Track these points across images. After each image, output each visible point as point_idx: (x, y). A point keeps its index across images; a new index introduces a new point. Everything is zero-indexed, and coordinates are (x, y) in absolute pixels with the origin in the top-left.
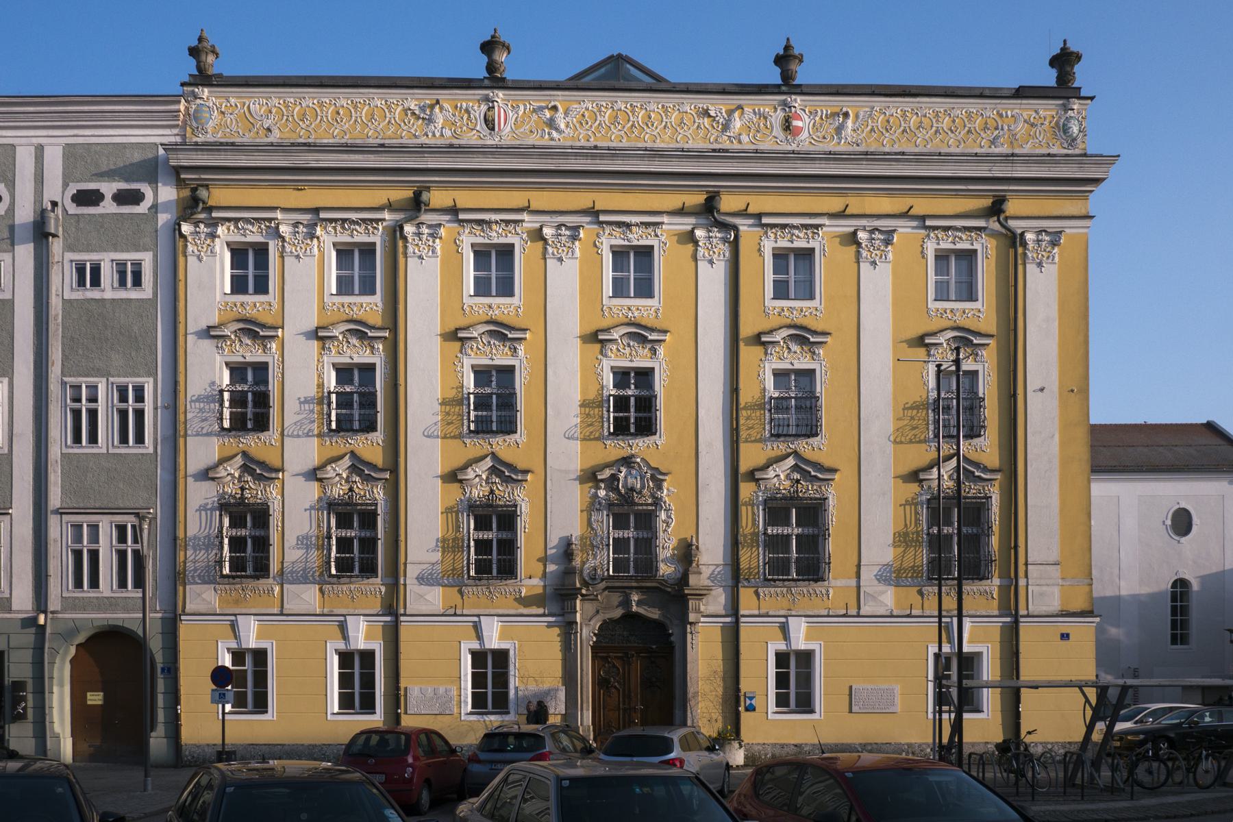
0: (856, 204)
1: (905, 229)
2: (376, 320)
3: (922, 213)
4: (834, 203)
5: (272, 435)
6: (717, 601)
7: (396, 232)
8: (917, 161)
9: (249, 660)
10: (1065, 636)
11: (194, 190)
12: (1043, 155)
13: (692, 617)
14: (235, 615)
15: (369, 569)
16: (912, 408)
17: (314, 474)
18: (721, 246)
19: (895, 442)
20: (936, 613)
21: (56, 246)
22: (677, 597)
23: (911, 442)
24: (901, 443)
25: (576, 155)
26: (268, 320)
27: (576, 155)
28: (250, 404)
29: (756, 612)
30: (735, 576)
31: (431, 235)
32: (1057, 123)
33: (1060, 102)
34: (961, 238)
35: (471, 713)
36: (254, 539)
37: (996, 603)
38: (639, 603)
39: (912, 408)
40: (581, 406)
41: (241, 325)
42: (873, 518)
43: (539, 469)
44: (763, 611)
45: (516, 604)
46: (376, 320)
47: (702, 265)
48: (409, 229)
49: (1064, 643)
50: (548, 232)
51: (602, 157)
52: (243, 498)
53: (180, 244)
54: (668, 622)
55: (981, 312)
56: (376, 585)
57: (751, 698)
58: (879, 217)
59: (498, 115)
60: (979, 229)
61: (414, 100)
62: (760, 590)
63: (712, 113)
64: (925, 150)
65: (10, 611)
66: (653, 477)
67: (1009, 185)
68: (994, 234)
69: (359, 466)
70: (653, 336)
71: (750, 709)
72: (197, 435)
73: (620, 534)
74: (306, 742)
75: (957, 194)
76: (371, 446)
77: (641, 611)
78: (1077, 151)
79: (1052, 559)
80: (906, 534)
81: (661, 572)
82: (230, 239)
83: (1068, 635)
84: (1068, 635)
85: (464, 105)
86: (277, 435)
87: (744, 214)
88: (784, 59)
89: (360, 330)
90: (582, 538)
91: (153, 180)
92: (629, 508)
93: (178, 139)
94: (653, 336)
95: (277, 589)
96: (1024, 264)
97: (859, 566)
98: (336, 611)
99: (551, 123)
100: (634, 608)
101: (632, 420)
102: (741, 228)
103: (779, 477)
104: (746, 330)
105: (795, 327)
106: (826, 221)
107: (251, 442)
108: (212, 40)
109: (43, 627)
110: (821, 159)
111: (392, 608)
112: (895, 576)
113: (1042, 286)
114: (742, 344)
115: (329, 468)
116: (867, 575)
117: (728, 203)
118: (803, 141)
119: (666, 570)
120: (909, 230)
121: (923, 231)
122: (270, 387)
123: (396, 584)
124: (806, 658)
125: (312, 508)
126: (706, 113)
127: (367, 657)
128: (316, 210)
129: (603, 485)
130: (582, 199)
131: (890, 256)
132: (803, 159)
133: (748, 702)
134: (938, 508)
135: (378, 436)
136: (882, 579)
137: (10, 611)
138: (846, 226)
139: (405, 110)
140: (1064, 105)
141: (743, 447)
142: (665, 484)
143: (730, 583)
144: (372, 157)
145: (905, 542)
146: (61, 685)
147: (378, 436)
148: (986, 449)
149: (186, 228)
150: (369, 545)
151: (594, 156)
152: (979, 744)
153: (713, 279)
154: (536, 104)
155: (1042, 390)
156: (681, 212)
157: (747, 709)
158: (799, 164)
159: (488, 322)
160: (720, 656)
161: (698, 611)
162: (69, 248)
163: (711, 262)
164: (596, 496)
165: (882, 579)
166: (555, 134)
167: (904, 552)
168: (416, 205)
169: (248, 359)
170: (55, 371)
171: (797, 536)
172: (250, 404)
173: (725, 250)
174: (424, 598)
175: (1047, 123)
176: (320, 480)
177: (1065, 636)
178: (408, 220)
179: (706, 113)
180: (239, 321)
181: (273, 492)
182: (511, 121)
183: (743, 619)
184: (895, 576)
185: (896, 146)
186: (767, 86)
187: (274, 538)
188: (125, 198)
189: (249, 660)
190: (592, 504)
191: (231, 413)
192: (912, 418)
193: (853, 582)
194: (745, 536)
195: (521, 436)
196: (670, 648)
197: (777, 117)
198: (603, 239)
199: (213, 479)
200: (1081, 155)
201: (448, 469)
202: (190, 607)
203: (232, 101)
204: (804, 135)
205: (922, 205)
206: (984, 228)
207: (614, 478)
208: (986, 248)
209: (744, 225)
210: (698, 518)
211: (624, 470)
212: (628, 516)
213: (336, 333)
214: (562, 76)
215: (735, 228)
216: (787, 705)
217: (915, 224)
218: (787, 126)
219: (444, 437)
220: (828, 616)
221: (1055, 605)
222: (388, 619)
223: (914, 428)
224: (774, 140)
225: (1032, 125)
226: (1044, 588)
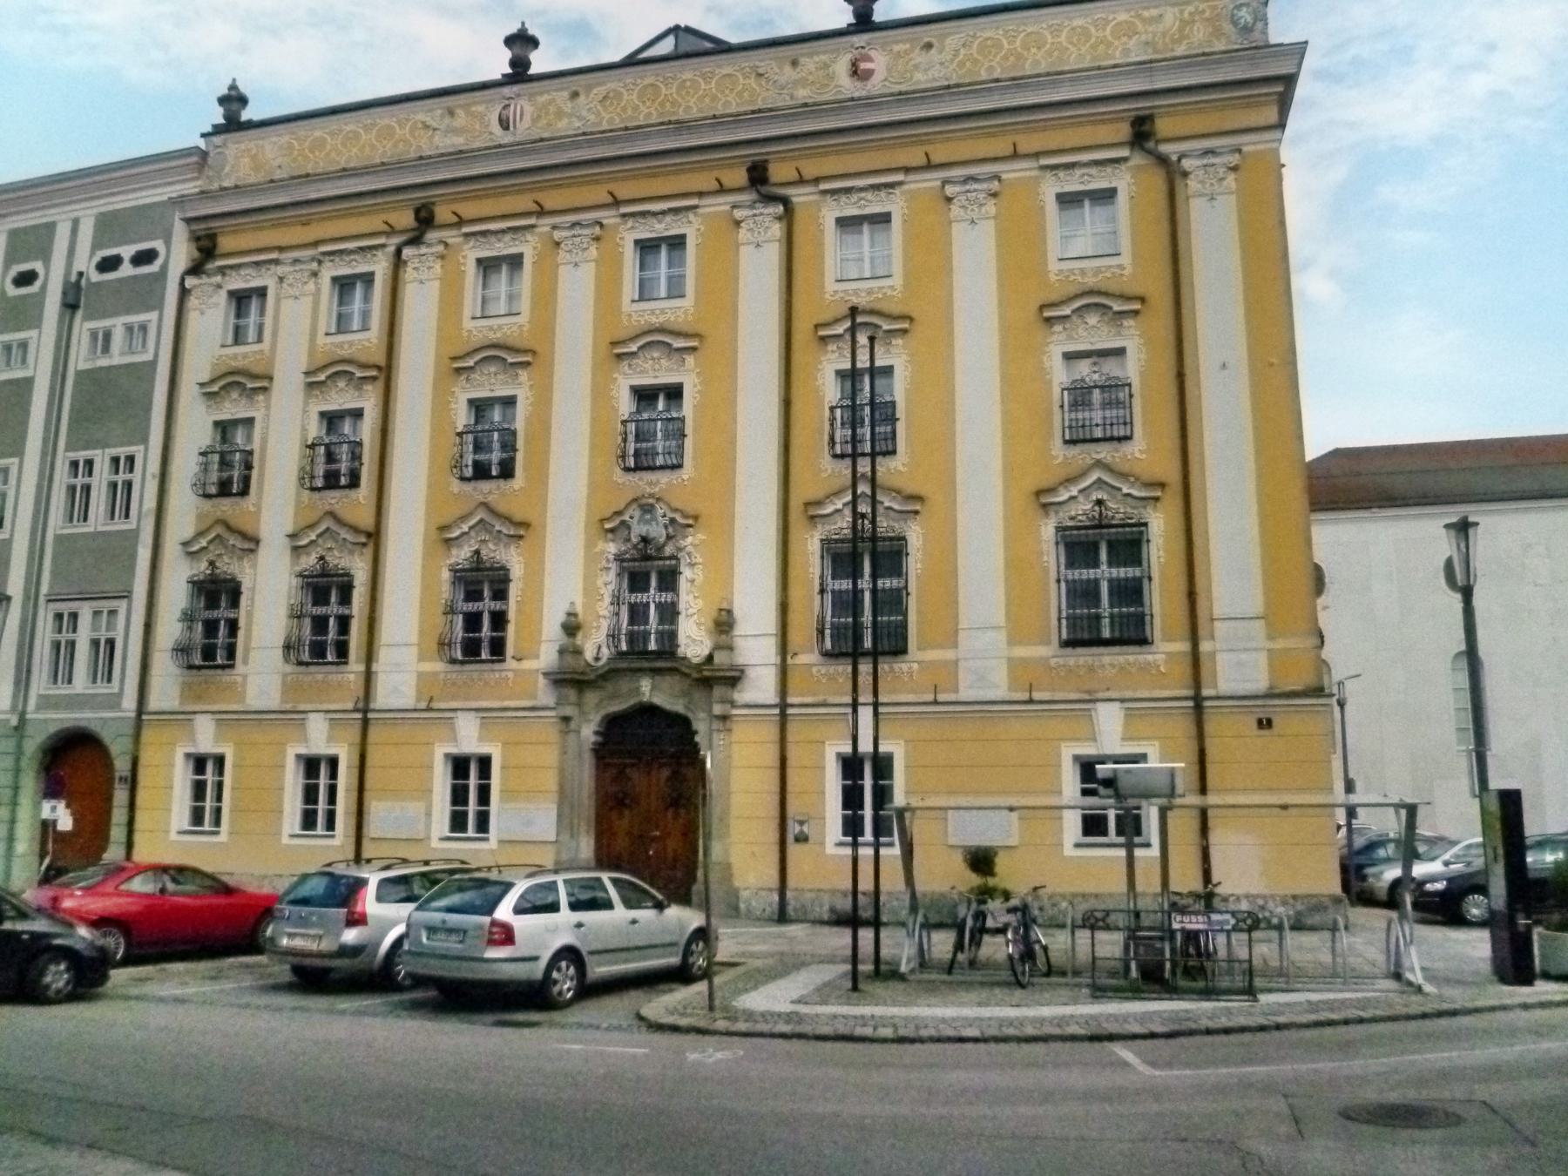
15: (1134, 634)
20: (848, 699)
35: (1078, 845)
36: (659, 606)
54: (690, 715)
57: (801, 823)
71: (802, 839)
73: (471, 607)
75: (1078, 122)
84: (1269, 723)
88: (521, 42)
98: (831, 700)
102: (795, 200)
105: (1091, 292)
107: (225, 506)
113: (1213, 224)
117: (779, 172)
118: (875, 85)
124: (485, 763)
133: (797, 828)
134: (1078, 547)
148: (1146, 450)
150: (1130, 592)
155: (1224, 366)
157: (797, 840)
162: (87, 318)
168: (425, 220)
204: (876, 79)
209: (799, 196)
212: (647, 576)
215: (785, 201)
224: (847, 86)
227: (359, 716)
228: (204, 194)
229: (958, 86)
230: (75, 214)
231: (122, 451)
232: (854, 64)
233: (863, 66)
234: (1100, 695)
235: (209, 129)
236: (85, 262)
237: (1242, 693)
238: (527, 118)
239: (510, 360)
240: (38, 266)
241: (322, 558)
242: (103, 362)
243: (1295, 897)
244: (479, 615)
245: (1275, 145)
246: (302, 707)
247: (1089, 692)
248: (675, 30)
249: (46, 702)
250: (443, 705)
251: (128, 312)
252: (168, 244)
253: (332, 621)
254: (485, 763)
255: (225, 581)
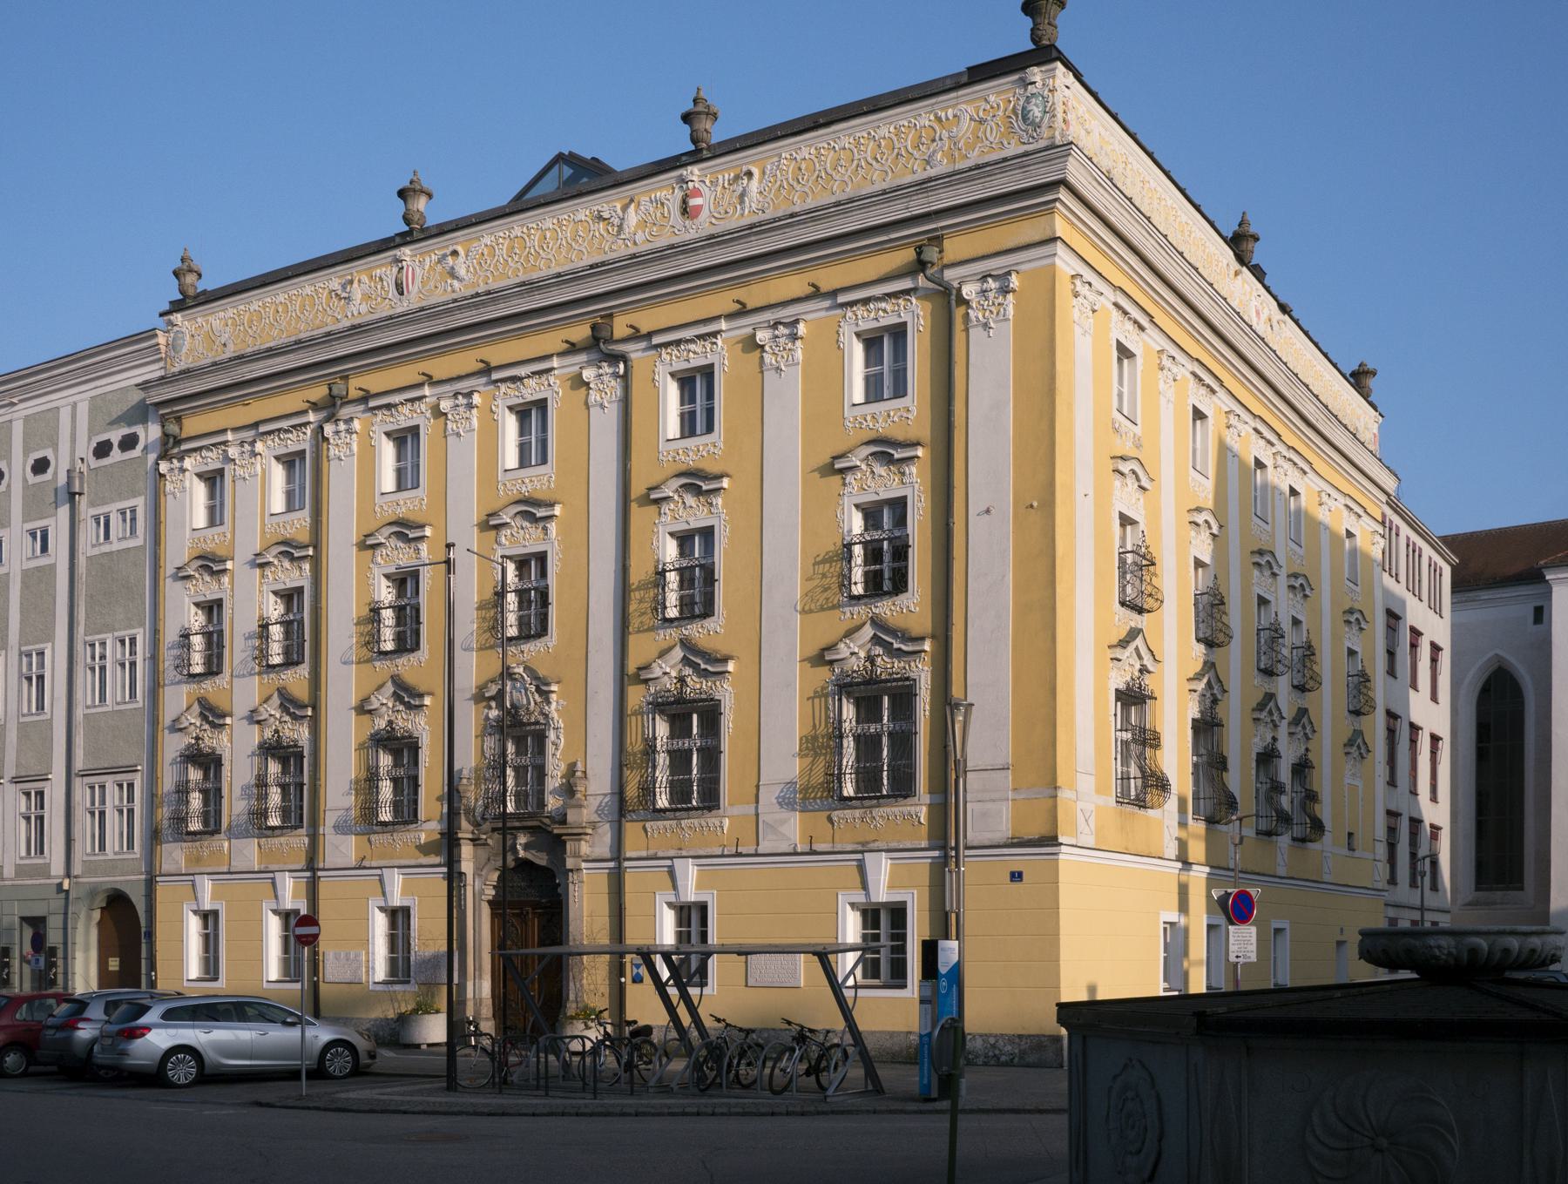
0: (754, 295)
1: (814, 312)
2: (304, 537)
3: (251, 421)
4: (724, 301)
5: (223, 680)
6: (598, 844)
7: (320, 437)
8: (813, 219)
9: (884, 919)
10: (1016, 876)
11: (919, 251)
12: (971, 169)
13: (570, 863)
14: (671, 858)
16: (824, 561)
17: (253, 718)
18: (613, 383)
19: (803, 612)
21: (83, 502)
22: (554, 838)
23: (822, 609)
24: (811, 611)
25: (459, 308)
26: (221, 552)
27: (459, 308)
28: (887, 558)
29: (644, 854)
30: (621, 809)
31: (347, 431)
32: (1014, 111)
33: (1015, 77)
34: (885, 311)
37: (924, 830)
38: (526, 847)
39: (824, 561)
40: (478, 609)
41: (200, 563)
42: (774, 720)
43: (441, 692)
44: (651, 852)
45: (417, 853)
46: (304, 537)
47: (594, 411)
48: (329, 429)
49: (1016, 885)
50: (762, 336)
51: (483, 304)
52: (199, 750)
53: (959, 312)
55: (910, 412)
56: (299, 840)
58: (460, 378)
59: (408, 277)
60: (907, 292)
61: (332, 280)
62: (648, 825)
63: (606, 215)
64: (885, 186)
65: (49, 877)
66: (538, 690)
67: (1042, 195)
68: (926, 296)
69: (289, 703)
70: (540, 513)
72: (639, 631)
74: (1009, 1030)
75: (881, 248)
76: (296, 680)
77: (529, 856)
78: (1042, 144)
79: (999, 762)
80: (815, 738)
81: (549, 808)
82: (198, 470)
83: (1020, 874)
84: (1020, 874)
85: (950, 112)
86: (227, 678)
87: (636, 336)
89: (886, 450)
90: (477, 769)
91: (144, 420)
92: (519, 731)
93: (162, 373)
94: (540, 513)
95: (226, 844)
96: (967, 330)
97: (758, 787)
98: (660, 854)
99: (452, 274)
100: (522, 854)
101: (886, 575)
102: (633, 356)
103: (667, 671)
104: (637, 489)
106: (723, 325)
108: (714, 101)
109: (67, 892)
110: (702, 247)
111: (945, 835)
112: (802, 798)
113: (989, 359)
114: (634, 506)
115: (842, 645)
116: (768, 797)
119: (552, 803)
120: (823, 314)
121: (839, 311)
122: (909, 531)
123: (945, 805)
124: (703, 908)
125: (253, 754)
126: (600, 218)
127: (898, 913)
128: (256, 425)
129: (493, 704)
130: (466, 361)
131: (799, 355)
132: (683, 252)
135: (304, 670)
136: (786, 803)
137: (49, 877)
138: (744, 326)
139: (331, 292)
140: (1021, 79)
141: (633, 640)
142: (554, 697)
143: (616, 817)
144: (291, 356)
145: (813, 749)
146: (87, 950)
147: (304, 670)
149: (164, 467)
151: (476, 306)
152: (899, 1033)
153: (605, 424)
154: (440, 253)
155: (988, 511)
156: (573, 349)
157: (634, 981)
158: (682, 260)
159: (868, 443)
160: (607, 912)
161: (577, 855)
162: (92, 504)
163: (602, 406)
164: (487, 718)
165: (786, 803)
166: (456, 283)
167: (813, 763)
169: (693, 526)
170: (80, 630)
171: (890, 734)
172: (887, 558)
173: (615, 386)
174: (341, 849)
175: (1000, 113)
176: (259, 722)
177: (1016, 876)
178: (327, 420)
179: (600, 218)
180: (868, 443)
181: (224, 737)
182: (418, 279)
183: (627, 864)
184: (802, 798)
185: (809, 200)
186: (391, 239)
187: (225, 792)
188: (129, 443)
189: (884, 919)
190: (485, 728)
191: (866, 574)
192: (824, 576)
193: (751, 809)
194: (635, 754)
195: (424, 653)
196: (560, 903)
197: (673, 199)
198: (499, 401)
199: (180, 730)
200: (1046, 149)
201: (813, 650)
202: (973, 836)
203: (992, 98)
204: (705, 214)
205: (829, 277)
206: (915, 290)
207: (501, 693)
208: (917, 315)
209: (635, 351)
210: (584, 747)
211: (509, 683)
213: (855, 460)
214: (503, 199)
215: (624, 358)
216: (876, 975)
217: (827, 303)
218: (685, 210)
219: (359, 663)
220: (723, 856)
221: (1004, 830)
222: (936, 853)
223: (826, 590)
225: (981, 121)
226: (989, 805)
227: (308, 874)
228: (163, 381)
229: (851, 201)
230: (71, 400)
231: (126, 634)
232: (684, 202)
233: (693, 202)
234: (872, 846)
235: (167, 307)
236: (85, 448)
237: (987, 843)
238: (418, 279)
239: (897, 456)
240: (48, 453)
241: (277, 731)
242: (106, 548)
243: (1020, 1036)
244: (526, 767)
245: (1048, 261)
246: (272, 868)
247: (863, 844)
248: (560, 159)
249: (90, 868)
250: (374, 864)
251: (121, 498)
252: (56, 450)
253: (885, 740)
254: (703, 908)
255: (403, 738)
